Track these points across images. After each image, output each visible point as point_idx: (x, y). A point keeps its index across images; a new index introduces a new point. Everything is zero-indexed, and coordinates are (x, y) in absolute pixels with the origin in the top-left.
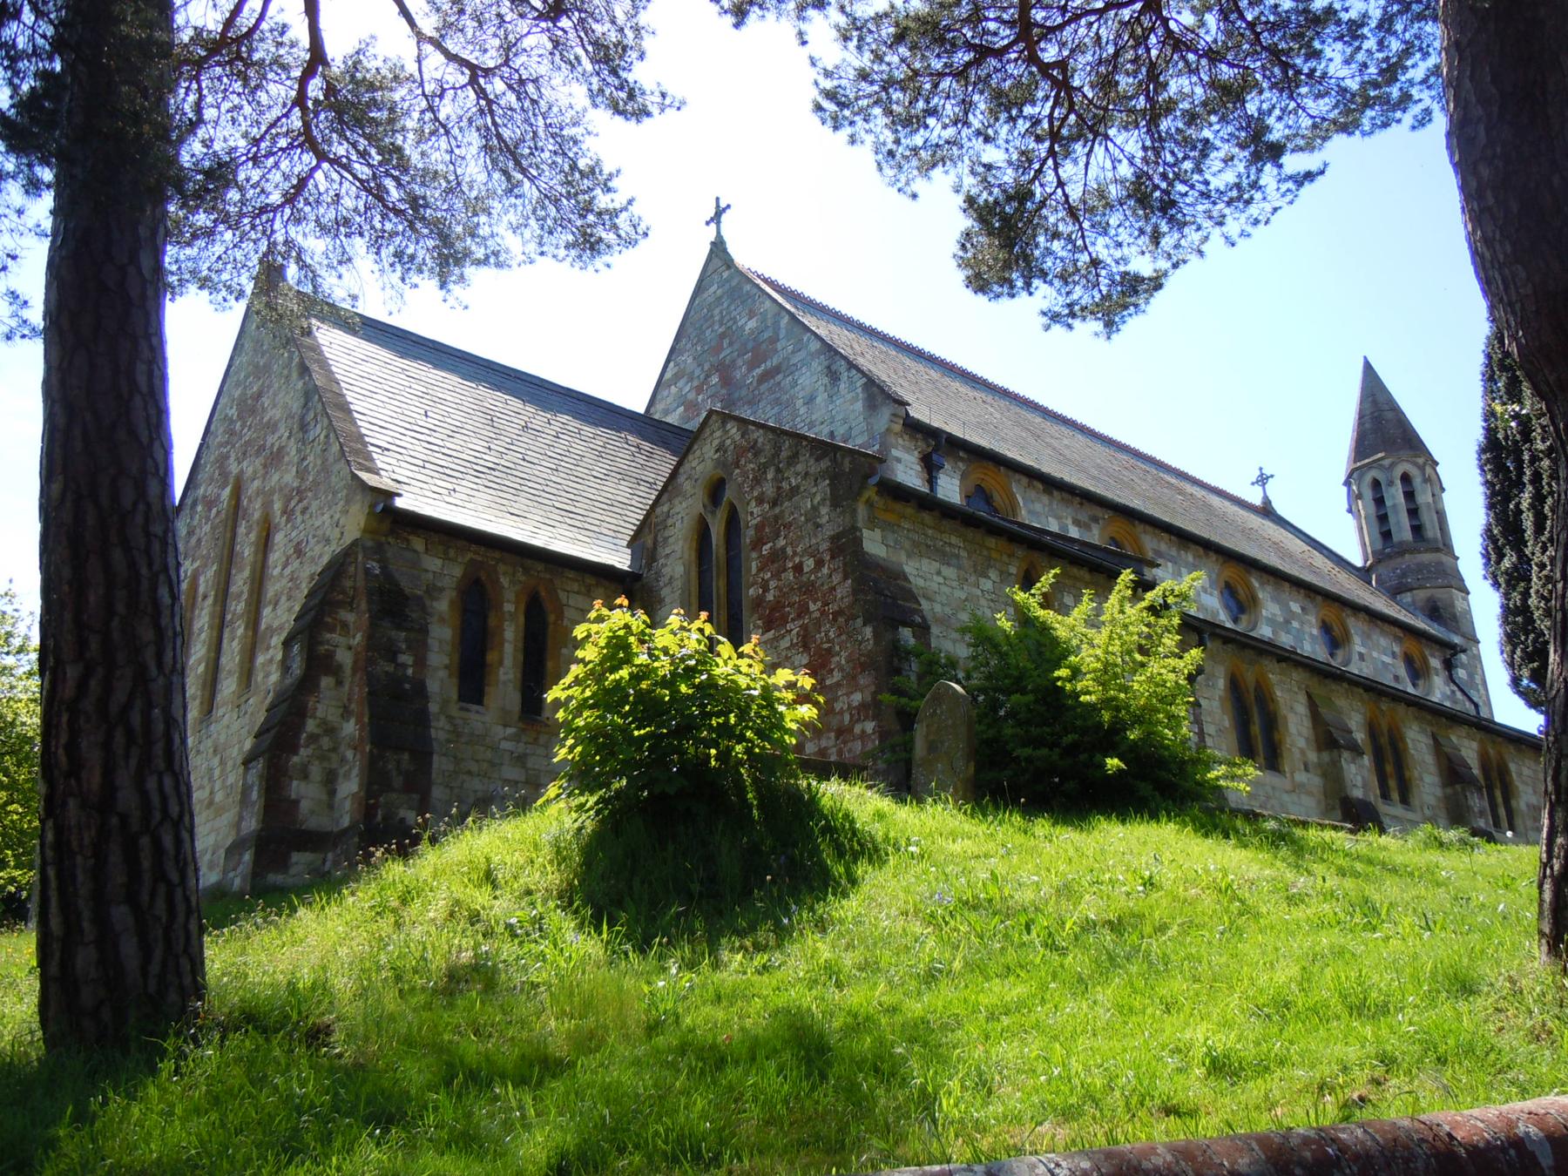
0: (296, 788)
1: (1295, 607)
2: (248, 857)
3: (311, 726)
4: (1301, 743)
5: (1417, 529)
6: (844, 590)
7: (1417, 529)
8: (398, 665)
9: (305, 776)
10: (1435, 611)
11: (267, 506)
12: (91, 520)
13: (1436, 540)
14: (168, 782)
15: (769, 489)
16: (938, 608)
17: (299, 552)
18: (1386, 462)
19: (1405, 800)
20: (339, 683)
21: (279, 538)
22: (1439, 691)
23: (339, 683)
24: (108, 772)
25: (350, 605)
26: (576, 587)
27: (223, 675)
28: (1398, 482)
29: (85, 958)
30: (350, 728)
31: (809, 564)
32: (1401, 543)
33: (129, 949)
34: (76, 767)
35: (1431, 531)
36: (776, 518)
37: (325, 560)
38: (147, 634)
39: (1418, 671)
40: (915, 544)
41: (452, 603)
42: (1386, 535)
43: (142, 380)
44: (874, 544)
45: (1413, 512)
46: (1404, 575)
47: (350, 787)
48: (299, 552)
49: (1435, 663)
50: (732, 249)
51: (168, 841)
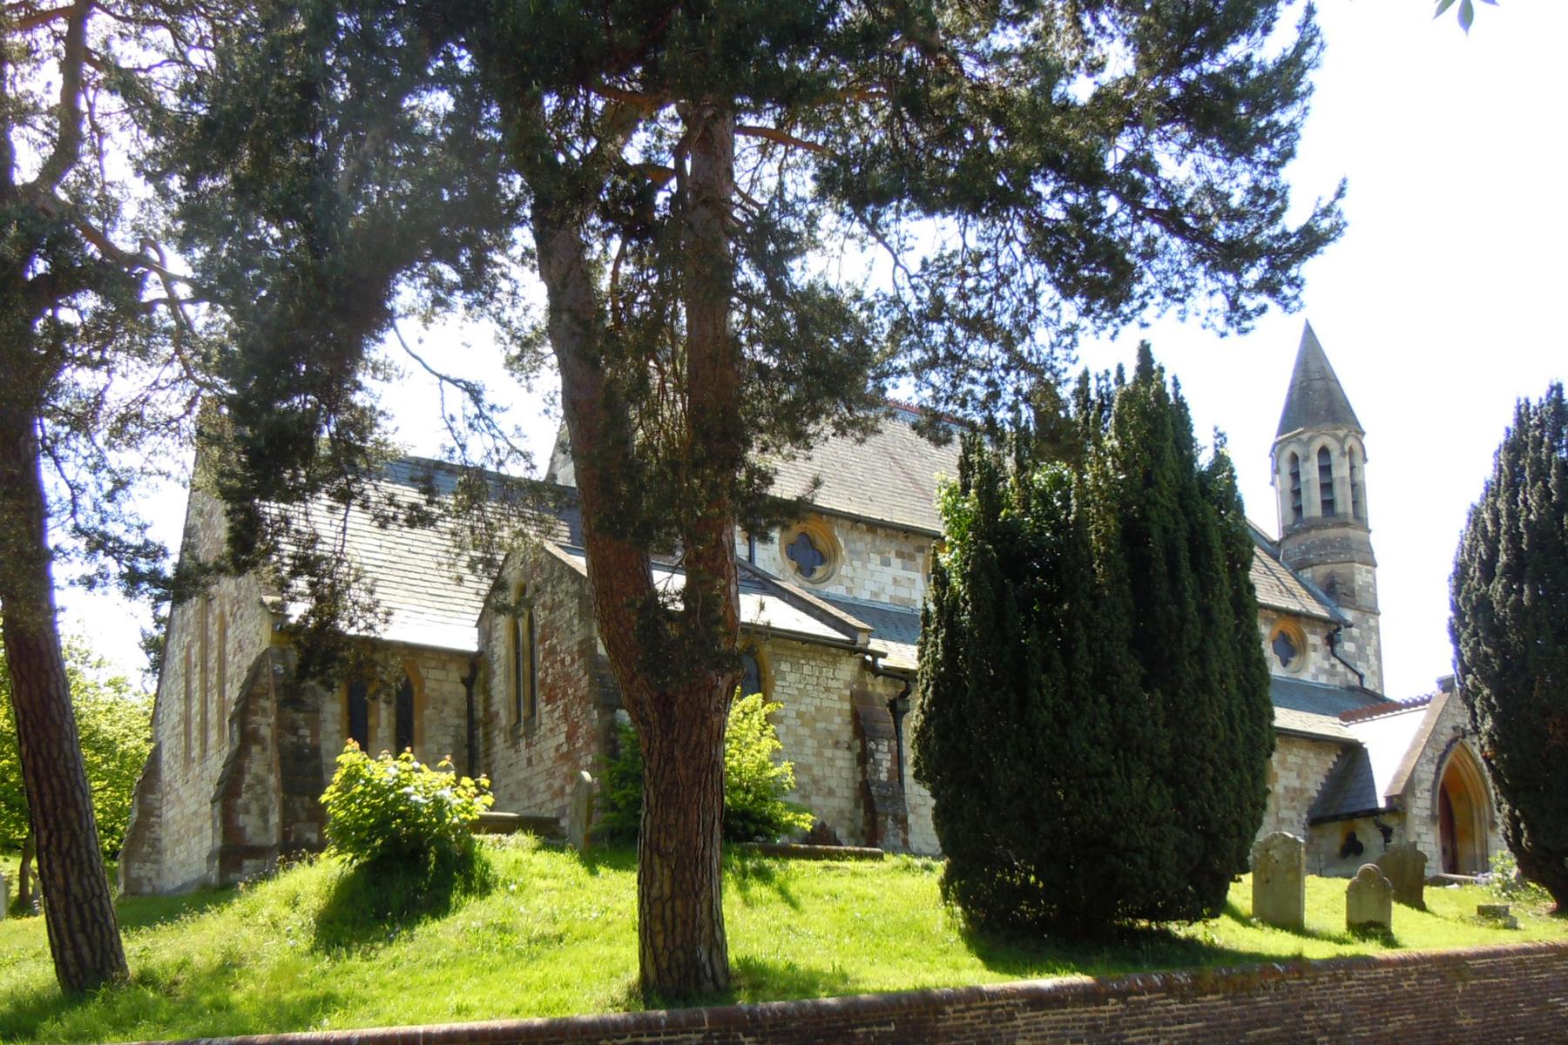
0: (242, 820)
2: (217, 863)
3: (248, 779)
5: (1328, 504)
7: (1328, 504)
10: (1333, 590)
12: (41, 764)
13: (1346, 515)
14: (93, 879)
18: (1305, 437)
20: (264, 749)
21: (230, 632)
23: (264, 749)
24: (66, 877)
25: (266, 695)
26: (433, 664)
28: (1315, 458)
29: (69, 954)
30: (273, 780)
32: (1310, 519)
33: (86, 951)
34: (52, 875)
35: (1344, 504)
36: (553, 622)
38: (73, 815)
42: (1298, 510)
43: (53, 692)
45: (1327, 487)
46: (1308, 551)
47: (275, 819)
51: (96, 905)
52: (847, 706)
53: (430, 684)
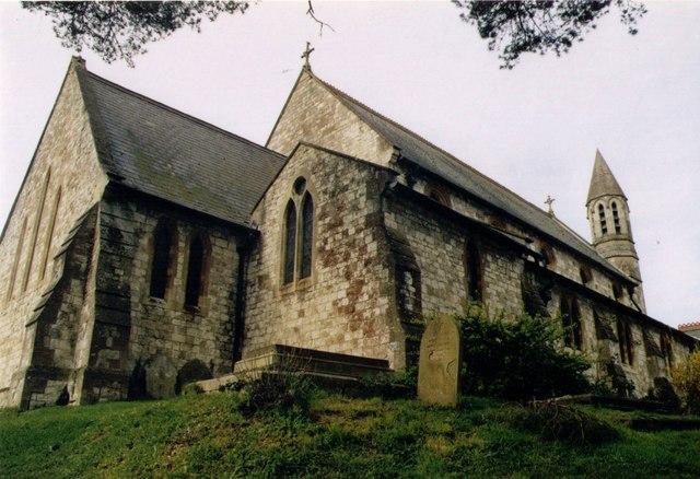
0: (53, 343)
1: (571, 263)
3: (64, 307)
4: (591, 336)
5: (618, 229)
6: (372, 247)
7: (618, 229)
8: (115, 275)
9: (59, 336)
11: (61, 181)
15: (330, 187)
16: (424, 260)
17: (72, 208)
19: (631, 363)
21: (64, 199)
22: (626, 302)
27: (32, 271)
31: (352, 231)
37: (83, 212)
39: (618, 294)
40: (413, 223)
41: (150, 240)
44: (390, 221)
45: (616, 221)
48: (72, 208)
49: (625, 291)
50: (315, 70)
52: (519, 291)
53: (215, 249)
